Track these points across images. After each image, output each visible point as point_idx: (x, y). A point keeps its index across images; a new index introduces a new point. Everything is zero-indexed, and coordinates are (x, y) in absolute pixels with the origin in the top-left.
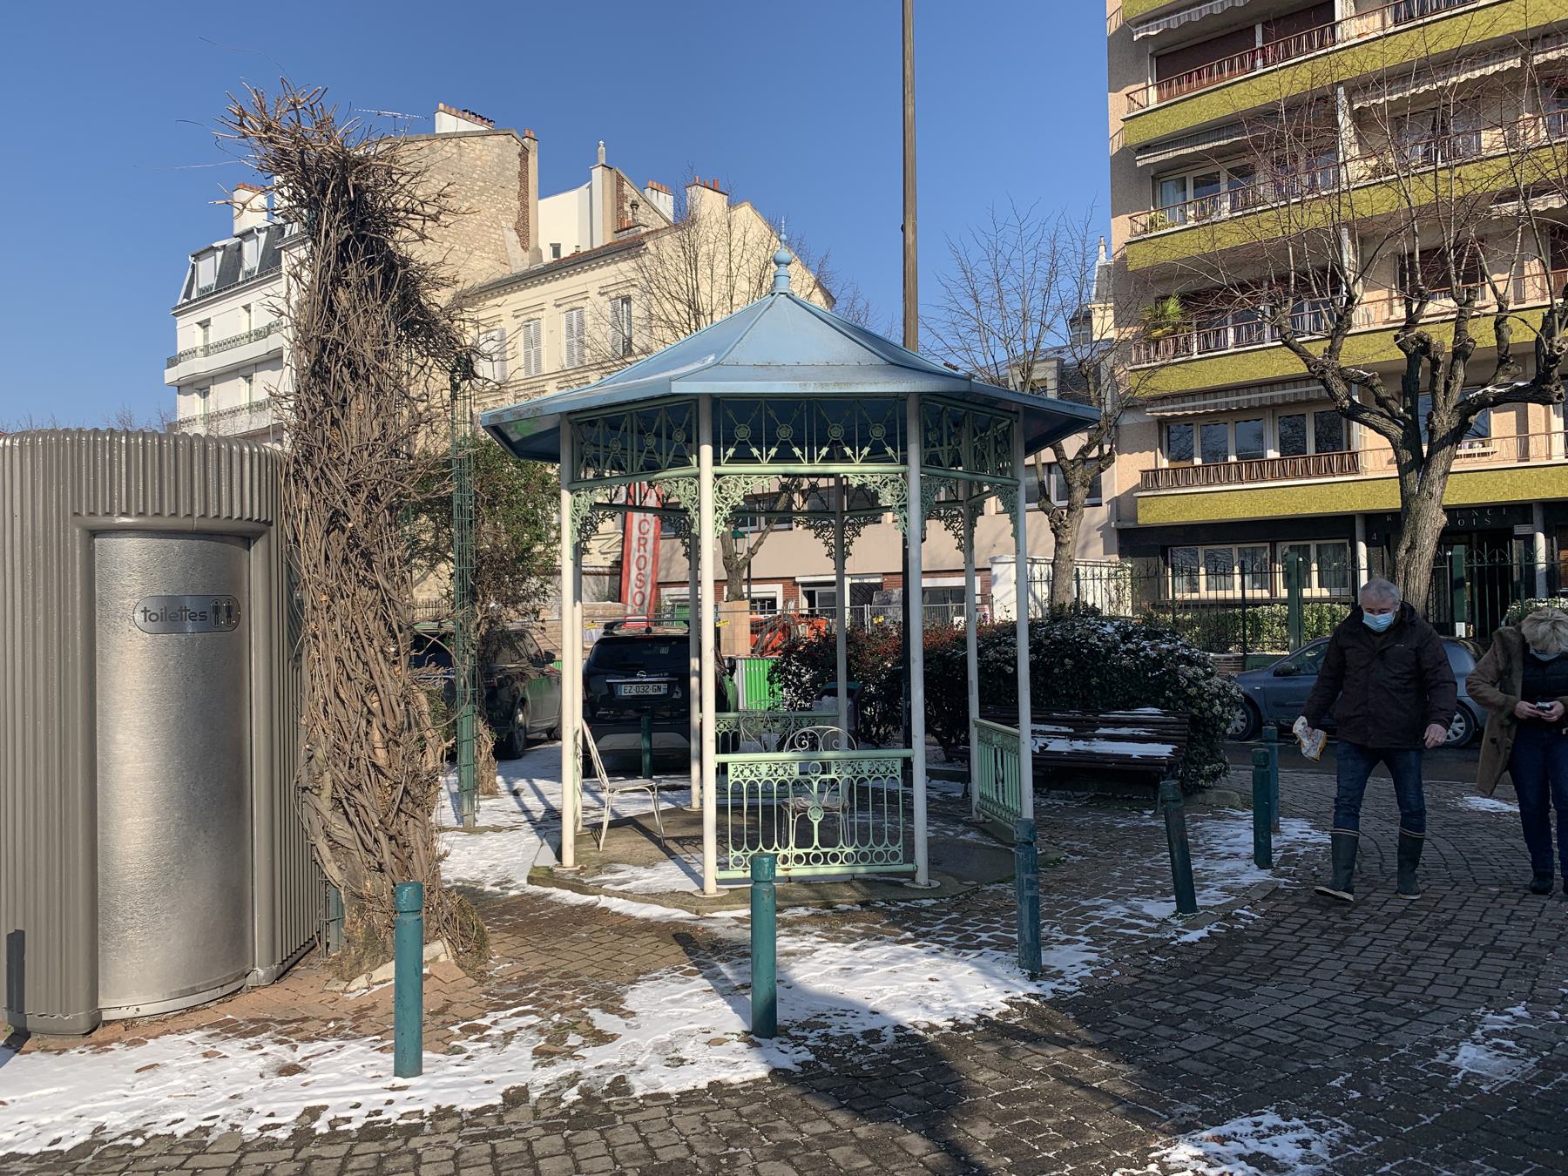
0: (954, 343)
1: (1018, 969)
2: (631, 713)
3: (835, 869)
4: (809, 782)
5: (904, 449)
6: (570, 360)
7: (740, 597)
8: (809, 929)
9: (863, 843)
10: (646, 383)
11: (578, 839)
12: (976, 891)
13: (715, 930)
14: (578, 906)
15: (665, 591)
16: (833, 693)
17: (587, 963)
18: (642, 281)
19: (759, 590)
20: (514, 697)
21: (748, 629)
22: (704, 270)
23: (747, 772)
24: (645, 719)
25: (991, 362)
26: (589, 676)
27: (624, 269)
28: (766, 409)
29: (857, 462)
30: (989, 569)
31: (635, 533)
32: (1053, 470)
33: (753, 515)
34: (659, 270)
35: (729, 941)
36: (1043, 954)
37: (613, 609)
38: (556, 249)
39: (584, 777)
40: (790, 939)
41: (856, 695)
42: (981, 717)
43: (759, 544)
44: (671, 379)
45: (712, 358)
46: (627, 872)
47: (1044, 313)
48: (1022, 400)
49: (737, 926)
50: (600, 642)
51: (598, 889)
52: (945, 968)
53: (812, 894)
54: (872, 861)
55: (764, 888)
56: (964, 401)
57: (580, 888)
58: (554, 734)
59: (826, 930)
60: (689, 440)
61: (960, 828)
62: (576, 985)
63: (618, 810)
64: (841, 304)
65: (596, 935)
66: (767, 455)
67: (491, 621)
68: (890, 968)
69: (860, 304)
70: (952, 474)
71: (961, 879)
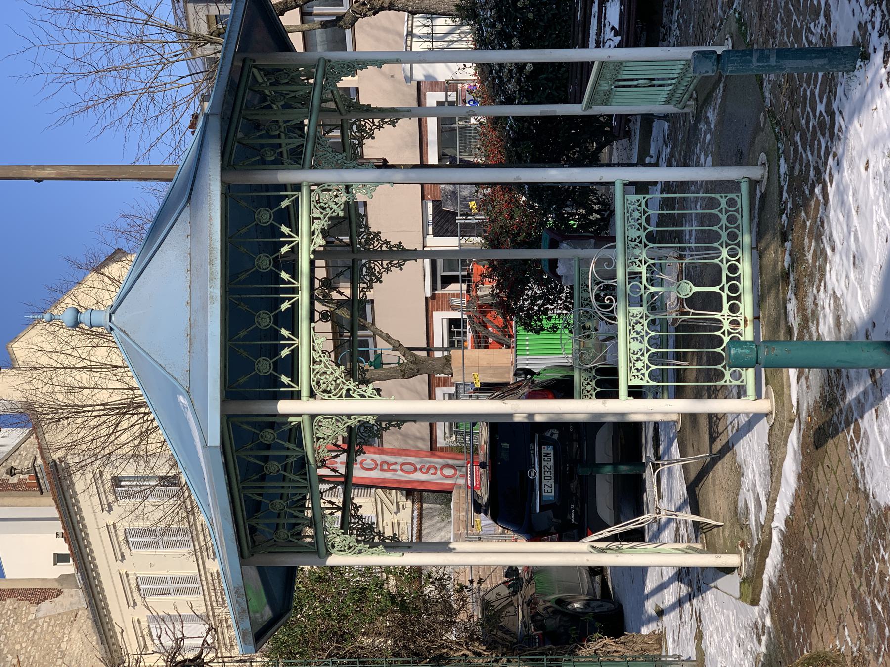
0: (166, 121)
1: (856, 72)
2: (574, 485)
3: (745, 268)
4: (652, 295)
5: (284, 187)
6: (180, 544)
7: (448, 359)
8: (810, 300)
9: (717, 236)
10: (208, 472)
11: (711, 549)
12: (771, 114)
13: (811, 402)
14: (783, 552)
15: (441, 442)
16: (553, 263)
17: (845, 544)
18: (96, 465)
19: (440, 338)
20: (555, 612)
21: (482, 352)
22: (84, 397)
23: (639, 365)
24: (581, 471)
25: (189, 80)
26: (535, 535)
27: (81, 483)
28: (239, 340)
29: (297, 239)
30: (419, 83)
31: (376, 474)
32: (309, 10)
33: (356, 344)
34: (84, 447)
35: (823, 388)
36: (840, 44)
37: (460, 501)
38: (60, 558)
39: (643, 541)
40: (821, 321)
41: (557, 238)
42: (581, 102)
43: (388, 339)
44: (205, 446)
45: (181, 399)
46: (747, 497)
47: (134, 21)
48: (230, 56)
49: (807, 379)
50: (495, 518)
51: (766, 529)
52: (854, 153)
53: (773, 295)
54: (737, 228)
55: (764, 353)
56: (231, 119)
57: (764, 549)
58: (596, 571)
59: (812, 281)
60: (272, 426)
61: (702, 127)
62: (869, 558)
63: (679, 502)
64: (122, 244)
65: (815, 534)
66: (289, 339)
67: (471, 638)
68: (854, 212)
69: (123, 224)
70: (312, 133)
71: (758, 130)
